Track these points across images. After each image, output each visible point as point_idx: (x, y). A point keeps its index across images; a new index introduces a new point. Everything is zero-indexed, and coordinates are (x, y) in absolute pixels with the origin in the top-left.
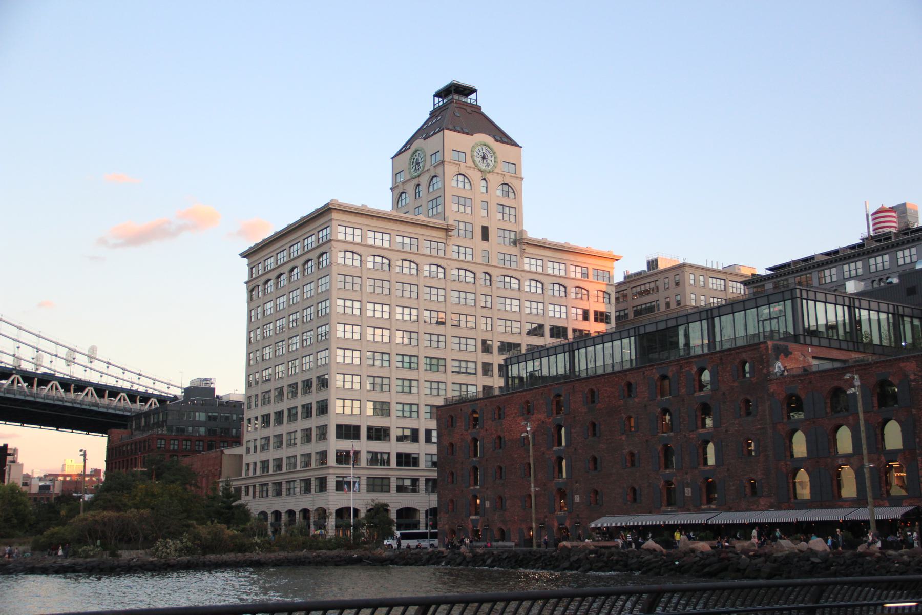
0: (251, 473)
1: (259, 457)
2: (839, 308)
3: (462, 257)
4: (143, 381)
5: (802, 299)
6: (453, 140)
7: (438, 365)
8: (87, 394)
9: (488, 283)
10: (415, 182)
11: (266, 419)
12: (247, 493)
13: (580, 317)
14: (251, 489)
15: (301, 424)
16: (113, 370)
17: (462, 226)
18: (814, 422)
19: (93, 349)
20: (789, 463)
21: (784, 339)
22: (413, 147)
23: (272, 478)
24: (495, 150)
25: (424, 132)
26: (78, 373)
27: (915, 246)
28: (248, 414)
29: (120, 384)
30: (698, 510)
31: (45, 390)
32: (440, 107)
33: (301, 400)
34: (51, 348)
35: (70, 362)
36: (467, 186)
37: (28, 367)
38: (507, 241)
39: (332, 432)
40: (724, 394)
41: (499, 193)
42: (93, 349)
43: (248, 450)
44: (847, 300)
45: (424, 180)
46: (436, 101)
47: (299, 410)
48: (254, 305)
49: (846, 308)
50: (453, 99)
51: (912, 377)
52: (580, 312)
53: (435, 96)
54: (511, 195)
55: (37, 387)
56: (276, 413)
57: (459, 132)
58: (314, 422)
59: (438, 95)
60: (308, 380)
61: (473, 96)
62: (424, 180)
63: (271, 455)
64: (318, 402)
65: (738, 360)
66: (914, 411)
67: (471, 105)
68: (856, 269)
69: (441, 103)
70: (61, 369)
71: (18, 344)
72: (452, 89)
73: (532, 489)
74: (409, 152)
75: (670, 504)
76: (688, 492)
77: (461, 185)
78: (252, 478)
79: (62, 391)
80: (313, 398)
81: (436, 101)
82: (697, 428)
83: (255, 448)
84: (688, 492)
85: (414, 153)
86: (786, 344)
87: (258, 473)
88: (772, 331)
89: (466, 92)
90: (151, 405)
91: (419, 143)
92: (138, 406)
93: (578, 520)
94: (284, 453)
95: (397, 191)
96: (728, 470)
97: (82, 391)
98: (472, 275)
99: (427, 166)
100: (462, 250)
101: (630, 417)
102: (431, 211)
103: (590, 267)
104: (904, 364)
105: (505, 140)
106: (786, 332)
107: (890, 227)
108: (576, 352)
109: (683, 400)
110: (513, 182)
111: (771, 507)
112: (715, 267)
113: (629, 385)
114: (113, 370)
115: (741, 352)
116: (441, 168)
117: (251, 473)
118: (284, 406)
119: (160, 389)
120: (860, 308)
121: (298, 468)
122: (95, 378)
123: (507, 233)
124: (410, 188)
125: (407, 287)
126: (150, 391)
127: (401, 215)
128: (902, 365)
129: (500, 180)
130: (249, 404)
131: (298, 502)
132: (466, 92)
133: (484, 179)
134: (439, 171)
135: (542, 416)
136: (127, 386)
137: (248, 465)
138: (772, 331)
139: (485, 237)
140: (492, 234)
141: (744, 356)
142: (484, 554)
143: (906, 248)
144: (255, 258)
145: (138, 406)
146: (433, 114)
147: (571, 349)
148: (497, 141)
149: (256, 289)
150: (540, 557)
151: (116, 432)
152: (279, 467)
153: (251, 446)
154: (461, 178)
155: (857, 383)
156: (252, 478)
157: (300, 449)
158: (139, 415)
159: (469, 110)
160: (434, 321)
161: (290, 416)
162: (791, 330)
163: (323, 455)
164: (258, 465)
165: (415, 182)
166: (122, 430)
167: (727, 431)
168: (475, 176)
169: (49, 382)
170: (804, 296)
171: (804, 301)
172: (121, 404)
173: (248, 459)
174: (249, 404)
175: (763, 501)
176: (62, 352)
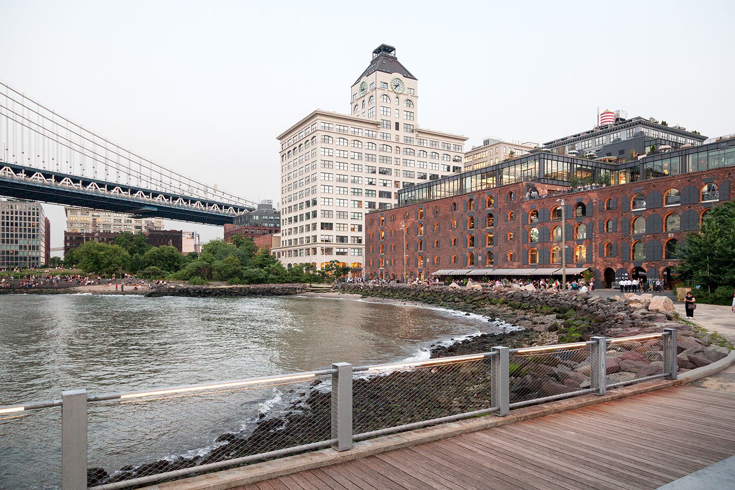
0: (284, 246)
1: (287, 238)
2: (565, 164)
3: (385, 139)
4: (240, 201)
5: (544, 159)
6: (381, 77)
7: (372, 194)
8: (214, 208)
9: (398, 152)
10: (362, 99)
11: (290, 219)
12: (283, 255)
13: (446, 170)
14: (284, 253)
15: (305, 222)
16: (225, 196)
17: (385, 122)
18: (543, 224)
19: (216, 186)
20: (529, 245)
21: (534, 181)
22: (362, 81)
23: (293, 248)
24: (403, 81)
25: (367, 73)
26: (210, 197)
27: (620, 132)
28: (283, 217)
29: (159, 190)
30: (484, 267)
31: (157, 199)
32: (376, 59)
33: (305, 210)
34: (196, 185)
35: (206, 192)
36: (388, 101)
37: (187, 194)
38: (408, 130)
39: (319, 226)
40: (500, 209)
41: (405, 105)
42: (216, 186)
43: (283, 234)
44: (570, 160)
45: (367, 98)
46: (374, 56)
47: (304, 215)
48: (284, 163)
49: (569, 164)
50: (382, 54)
51: (594, 201)
52: (446, 167)
53: (373, 53)
54: (411, 106)
55: (172, 201)
56: (294, 217)
57: (385, 72)
58: (311, 221)
59: (375, 52)
60: (308, 201)
61: (393, 52)
62: (367, 98)
63: (293, 237)
64: (313, 212)
65: (508, 192)
66: (593, 219)
67: (392, 57)
68: (588, 144)
69: (376, 56)
70: (202, 195)
71: (118, 171)
72: (382, 48)
73: (405, 256)
74: (360, 83)
75: (472, 263)
76: (480, 258)
77: (385, 100)
78: (284, 248)
79: (202, 206)
80: (311, 209)
81: (374, 56)
82: (486, 226)
83: (286, 233)
84: (480, 258)
85: (362, 84)
86: (533, 183)
87: (287, 246)
88: (528, 176)
89: (389, 50)
90: (214, 208)
91: (364, 79)
92: (239, 213)
93: (428, 271)
94: (298, 236)
95: (354, 105)
96: (500, 248)
97: (177, 200)
98: (390, 148)
99: (368, 91)
100: (385, 135)
101: (406, 212)
102: (370, 115)
103: (452, 144)
104: (591, 194)
105: (409, 76)
106: (535, 177)
107: (609, 121)
108: (432, 187)
109: (480, 212)
110: (413, 99)
111: (519, 267)
112: (517, 144)
113: (455, 204)
114: (225, 196)
115: (510, 187)
116: (375, 91)
117: (284, 246)
118: (298, 213)
119: (249, 205)
120: (576, 164)
121: (304, 243)
122: (218, 200)
123: (409, 126)
124: (360, 103)
125: (434, 165)
126: (244, 206)
127: (355, 116)
128: (589, 194)
129: (406, 97)
130: (283, 212)
131: (304, 259)
132: (389, 50)
133: (397, 97)
134: (374, 93)
135: (413, 220)
136: (233, 203)
137: (283, 241)
138: (528, 176)
139: (397, 128)
140: (401, 126)
141: (511, 189)
142: (378, 287)
143: (615, 133)
144: (283, 140)
145: (239, 213)
146: (372, 62)
147: (429, 186)
148: (404, 76)
149: (284, 156)
150: (403, 289)
151: (229, 226)
152: (302, 242)
153: (284, 232)
154: (385, 97)
155: (563, 204)
156: (284, 248)
157: (305, 234)
158: (240, 217)
159: (390, 60)
160: (370, 171)
161: (300, 218)
162: (537, 176)
163: (315, 237)
164: (287, 241)
165: (362, 99)
166: (229, 225)
167: (500, 228)
168: (393, 96)
169: (244, 210)
170: (546, 157)
171: (546, 160)
172: (230, 212)
173: (283, 239)
174: (283, 212)
175: (515, 264)
176: (202, 187)
